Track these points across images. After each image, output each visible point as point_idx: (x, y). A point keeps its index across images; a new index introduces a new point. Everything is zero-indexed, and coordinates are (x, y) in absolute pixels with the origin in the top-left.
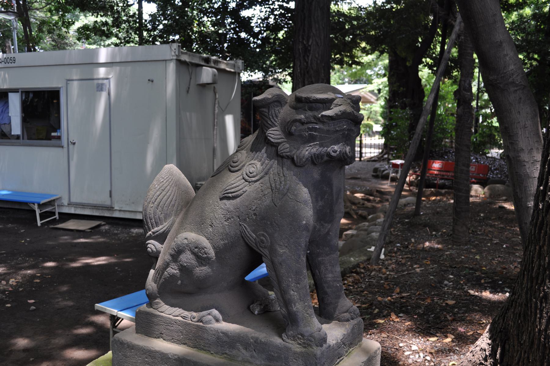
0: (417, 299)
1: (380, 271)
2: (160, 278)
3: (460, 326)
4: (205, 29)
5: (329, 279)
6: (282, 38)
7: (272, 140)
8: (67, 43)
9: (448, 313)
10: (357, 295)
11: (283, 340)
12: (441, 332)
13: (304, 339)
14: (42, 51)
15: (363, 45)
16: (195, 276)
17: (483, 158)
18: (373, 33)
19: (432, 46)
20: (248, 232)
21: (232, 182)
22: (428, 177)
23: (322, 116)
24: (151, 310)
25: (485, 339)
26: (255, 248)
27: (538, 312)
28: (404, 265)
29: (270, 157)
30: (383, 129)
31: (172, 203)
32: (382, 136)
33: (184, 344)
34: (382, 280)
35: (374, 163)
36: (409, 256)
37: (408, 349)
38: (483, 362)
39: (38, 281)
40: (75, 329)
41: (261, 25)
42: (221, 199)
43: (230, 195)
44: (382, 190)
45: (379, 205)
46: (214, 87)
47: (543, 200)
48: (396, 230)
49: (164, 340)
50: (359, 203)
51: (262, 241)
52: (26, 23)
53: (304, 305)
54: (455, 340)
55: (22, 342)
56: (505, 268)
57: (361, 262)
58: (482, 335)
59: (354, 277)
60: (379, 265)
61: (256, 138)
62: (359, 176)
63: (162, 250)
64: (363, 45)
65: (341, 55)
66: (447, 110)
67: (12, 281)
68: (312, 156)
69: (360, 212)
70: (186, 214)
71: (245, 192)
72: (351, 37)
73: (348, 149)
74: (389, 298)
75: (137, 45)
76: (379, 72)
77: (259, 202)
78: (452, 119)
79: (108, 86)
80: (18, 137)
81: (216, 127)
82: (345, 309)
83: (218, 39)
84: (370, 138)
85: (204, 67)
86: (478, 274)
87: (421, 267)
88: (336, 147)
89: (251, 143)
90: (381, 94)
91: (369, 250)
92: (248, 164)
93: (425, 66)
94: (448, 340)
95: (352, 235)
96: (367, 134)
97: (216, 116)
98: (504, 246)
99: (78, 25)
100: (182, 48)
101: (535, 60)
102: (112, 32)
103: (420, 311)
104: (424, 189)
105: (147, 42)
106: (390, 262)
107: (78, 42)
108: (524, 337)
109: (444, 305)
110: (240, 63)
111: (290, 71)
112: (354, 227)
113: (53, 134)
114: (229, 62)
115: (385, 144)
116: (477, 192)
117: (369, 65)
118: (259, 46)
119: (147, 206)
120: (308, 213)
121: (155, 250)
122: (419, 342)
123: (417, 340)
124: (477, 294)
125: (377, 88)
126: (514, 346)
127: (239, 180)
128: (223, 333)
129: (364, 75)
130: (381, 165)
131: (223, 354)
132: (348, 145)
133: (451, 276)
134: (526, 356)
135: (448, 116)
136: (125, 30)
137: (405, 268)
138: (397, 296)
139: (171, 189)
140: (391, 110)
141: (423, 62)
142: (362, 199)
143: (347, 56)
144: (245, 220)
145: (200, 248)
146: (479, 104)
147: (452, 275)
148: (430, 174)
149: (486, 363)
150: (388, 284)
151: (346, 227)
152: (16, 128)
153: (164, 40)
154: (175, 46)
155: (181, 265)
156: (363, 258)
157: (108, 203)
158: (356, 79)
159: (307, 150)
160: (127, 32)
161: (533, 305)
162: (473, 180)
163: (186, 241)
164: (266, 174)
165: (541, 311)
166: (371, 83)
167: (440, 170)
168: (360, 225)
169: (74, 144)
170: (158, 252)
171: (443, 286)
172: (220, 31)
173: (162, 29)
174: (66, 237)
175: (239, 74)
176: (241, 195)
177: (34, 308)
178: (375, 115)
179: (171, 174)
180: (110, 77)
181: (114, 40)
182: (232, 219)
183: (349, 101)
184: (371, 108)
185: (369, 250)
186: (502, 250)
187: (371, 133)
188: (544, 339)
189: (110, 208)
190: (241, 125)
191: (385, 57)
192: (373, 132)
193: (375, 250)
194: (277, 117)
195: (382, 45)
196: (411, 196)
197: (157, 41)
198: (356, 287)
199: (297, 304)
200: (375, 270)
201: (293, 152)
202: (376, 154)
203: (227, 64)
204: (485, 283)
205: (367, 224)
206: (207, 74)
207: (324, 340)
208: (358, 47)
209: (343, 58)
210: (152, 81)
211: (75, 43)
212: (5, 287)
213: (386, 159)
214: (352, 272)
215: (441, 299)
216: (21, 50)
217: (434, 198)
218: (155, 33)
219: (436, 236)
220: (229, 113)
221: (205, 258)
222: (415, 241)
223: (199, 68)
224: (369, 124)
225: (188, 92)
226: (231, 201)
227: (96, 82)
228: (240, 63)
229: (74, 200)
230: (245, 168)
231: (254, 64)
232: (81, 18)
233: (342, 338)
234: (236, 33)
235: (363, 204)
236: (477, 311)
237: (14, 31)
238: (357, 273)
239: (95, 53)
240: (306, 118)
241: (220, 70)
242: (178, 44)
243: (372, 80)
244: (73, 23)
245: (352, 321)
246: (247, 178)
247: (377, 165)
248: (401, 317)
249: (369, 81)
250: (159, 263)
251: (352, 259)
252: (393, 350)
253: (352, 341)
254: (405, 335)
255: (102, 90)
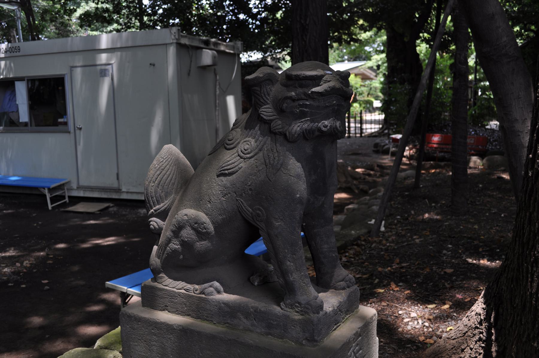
0: (416, 269)
1: (380, 242)
2: (163, 253)
3: (458, 293)
4: (203, 12)
5: (325, 250)
6: (280, 18)
7: (265, 117)
8: (70, 31)
9: (447, 281)
10: (358, 266)
11: (282, 309)
12: (439, 299)
13: (301, 307)
14: (46, 39)
15: (361, 22)
16: (196, 251)
17: (482, 130)
18: (371, 10)
19: (429, 21)
20: (245, 207)
21: (228, 159)
22: (428, 150)
23: (312, 92)
24: (156, 284)
25: (480, 304)
26: (252, 222)
27: (529, 276)
28: (404, 236)
29: (263, 134)
30: (383, 105)
31: (173, 181)
32: (382, 111)
33: (188, 315)
34: (382, 251)
35: (375, 138)
36: (409, 227)
37: (407, 316)
38: (478, 326)
39: (51, 262)
40: (88, 306)
41: (260, 6)
42: (218, 176)
43: (226, 172)
44: (383, 165)
45: (380, 180)
46: (215, 69)
47: (533, 168)
48: (397, 203)
49: (169, 312)
50: (360, 178)
51: (258, 215)
52: (29, 12)
53: (300, 275)
54: (453, 306)
55: (37, 320)
56: (503, 237)
57: (362, 235)
58: (477, 300)
59: (355, 249)
60: (380, 237)
61: (250, 116)
62: (360, 152)
63: (164, 226)
64: (361, 22)
65: (339, 33)
66: (445, 84)
67: (26, 263)
68: (303, 132)
69: (361, 186)
70: (185, 191)
71: (241, 168)
72: (349, 14)
73: (338, 124)
74: (389, 268)
75: (138, 30)
76: (378, 49)
77: (254, 177)
78: (450, 92)
79: (111, 72)
80: (26, 124)
81: (217, 108)
82: (341, 278)
83: (216, 21)
84: (370, 114)
85: (204, 50)
86: (476, 242)
87: (420, 237)
88: (326, 123)
89: (245, 121)
90: (381, 70)
91: (369, 222)
92: (242, 141)
93: (422, 41)
94: (446, 307)
95: (354, 210)
96: (368, 111)
97: (217, 97)
98: (503, 215)
99: (80, 12)
100: (182, 32)
101: (532, 31)
102: (113, 18)
103: (419, 280)
104: (423, 163)
105: (148, 27)
106: (390, 234)
107: (80, 29)
108: (517, 301)
109: (442, 273)
110: (239, 44)
111: (289, 51)
112: (356, 201)
113: (60, 120)
114: (229, 44)
115: (385, 119)
116: (475, 162)
117: (367, 42)
118: (257, 27)
119: (149, 185)
120: (301, 188)
121: (157, 227)
122: (418, 310)
123: (416, 307)
124: (474, 262)
125: (376, 64)
126: (507, 310)
127: (235, 157)
128: (224, 303)
129: (363, 52)
130: (381, 140)
131: (225, 323)
132: (338, 120)
133: (450, 246)
134: (519, 318)
135: (447, 90)
136: (125, 16)
137: (405, 239)
138: (397, 266)
139: (171, 168)
140: (390, 86)
141: (421, 37)
142: (363, 174)
143: (345, 34)
144: (241, 195)
145: (199, 224)
146: (478, 77)
147: (450, 244)
148: (430, 147)
149: (481, 327)
150: (388, 255)
151: (348, 202)
152: (24, 116)
153: (164, 25)
154: (174, 29)
155: (182, 240)
156: (364, 231)
157: (116, 185)
158: (356, 57)
159: (298, 126)
160: (127, 17)
161: (525, 270)
162: (473, 152)
163: (186, 217)
164: (260, 150)
165: (533, 275)
166: (370, 60)
167: (439, 143)
168: (361, 199)
169: (80, 129)
170: (161, 229)
171: (442, 255)
172: (219, 14)
173: (162, 14)
174: (76, 220)
175: (239, 55)
176: (237, 171)
177: (48, 288)
178: (375, 91)
179: (171, 154)
180: (112, 62)
181: (115, 26)
182: (229, 195)
183: (338, 77)
184: (371, 85)
185: (369, 222)
186: (500, 219)
187: (371, 109)
188: (536, 301)
189: (118, 190)
190: (243, 105)
191: (383, 33)
192: (373, 108)
193: (375, 222)
194: (269, 95)
195: (379, 22)
196: (411, 170)
197: (157, 25)
198: (357, 258)
199: (294, 274)
200: (375, 241)
201: (286, 128)
202: (376, 130)
203: (227, 46)
204: (483, 251)
205: (368, 198)
206: (207, 57)
207: (321, 307)
208: (356, 24)
209: (342, 36)
210: (154, 65)
211: (78, 30)
212: (20, 269)
213: (386, 134)
214: (353, 245)
215: (439, 268)
216: (25, 39)
217: (433, 171)
218: (156, 18)
219: (435, 207)
220: (230, 94)
221: (205, 233)
222: (415, 213)
223: (199, 51)
224: (369, 100)
225: (189, 74)
226: (228, 177)
227: (99, 68)
228: (239, 44)
229: (83, 183)
230: (240, 145)
231: (253, 44)
232: (82, 4)
233: (338, 305)
234: (235, 15)
235: (364, 179)
236: (474, 278)
237: (17, 20)
238: (358, 245)
239: (96, 39)
240: (297, 95)
241: (220, 52)
242: (177, 28)
243: (372, 56)
244: (75, 11)
245: (348, 289)
246: (242, 155)
247: (378, 140)
248: (401, 286)
249: (368, 58)
250: (162, 239)
251: (353, 232)
252: (393, 317)
253: (348, 309)
254: (404, 303)
255: (105, 75)
